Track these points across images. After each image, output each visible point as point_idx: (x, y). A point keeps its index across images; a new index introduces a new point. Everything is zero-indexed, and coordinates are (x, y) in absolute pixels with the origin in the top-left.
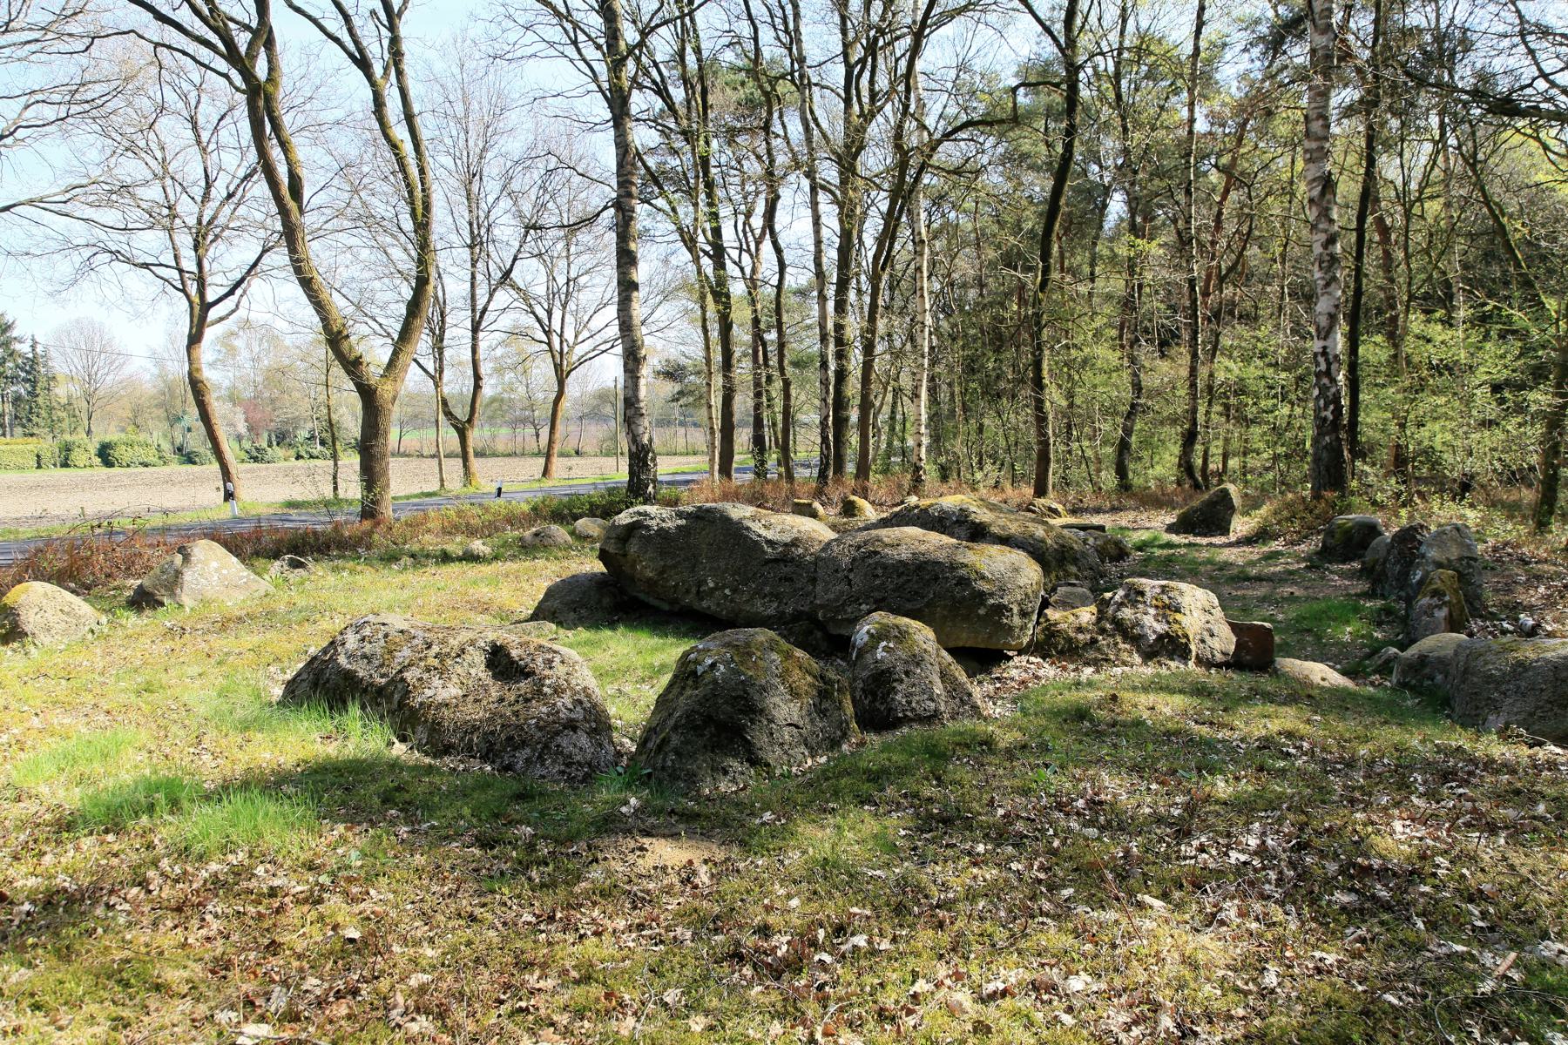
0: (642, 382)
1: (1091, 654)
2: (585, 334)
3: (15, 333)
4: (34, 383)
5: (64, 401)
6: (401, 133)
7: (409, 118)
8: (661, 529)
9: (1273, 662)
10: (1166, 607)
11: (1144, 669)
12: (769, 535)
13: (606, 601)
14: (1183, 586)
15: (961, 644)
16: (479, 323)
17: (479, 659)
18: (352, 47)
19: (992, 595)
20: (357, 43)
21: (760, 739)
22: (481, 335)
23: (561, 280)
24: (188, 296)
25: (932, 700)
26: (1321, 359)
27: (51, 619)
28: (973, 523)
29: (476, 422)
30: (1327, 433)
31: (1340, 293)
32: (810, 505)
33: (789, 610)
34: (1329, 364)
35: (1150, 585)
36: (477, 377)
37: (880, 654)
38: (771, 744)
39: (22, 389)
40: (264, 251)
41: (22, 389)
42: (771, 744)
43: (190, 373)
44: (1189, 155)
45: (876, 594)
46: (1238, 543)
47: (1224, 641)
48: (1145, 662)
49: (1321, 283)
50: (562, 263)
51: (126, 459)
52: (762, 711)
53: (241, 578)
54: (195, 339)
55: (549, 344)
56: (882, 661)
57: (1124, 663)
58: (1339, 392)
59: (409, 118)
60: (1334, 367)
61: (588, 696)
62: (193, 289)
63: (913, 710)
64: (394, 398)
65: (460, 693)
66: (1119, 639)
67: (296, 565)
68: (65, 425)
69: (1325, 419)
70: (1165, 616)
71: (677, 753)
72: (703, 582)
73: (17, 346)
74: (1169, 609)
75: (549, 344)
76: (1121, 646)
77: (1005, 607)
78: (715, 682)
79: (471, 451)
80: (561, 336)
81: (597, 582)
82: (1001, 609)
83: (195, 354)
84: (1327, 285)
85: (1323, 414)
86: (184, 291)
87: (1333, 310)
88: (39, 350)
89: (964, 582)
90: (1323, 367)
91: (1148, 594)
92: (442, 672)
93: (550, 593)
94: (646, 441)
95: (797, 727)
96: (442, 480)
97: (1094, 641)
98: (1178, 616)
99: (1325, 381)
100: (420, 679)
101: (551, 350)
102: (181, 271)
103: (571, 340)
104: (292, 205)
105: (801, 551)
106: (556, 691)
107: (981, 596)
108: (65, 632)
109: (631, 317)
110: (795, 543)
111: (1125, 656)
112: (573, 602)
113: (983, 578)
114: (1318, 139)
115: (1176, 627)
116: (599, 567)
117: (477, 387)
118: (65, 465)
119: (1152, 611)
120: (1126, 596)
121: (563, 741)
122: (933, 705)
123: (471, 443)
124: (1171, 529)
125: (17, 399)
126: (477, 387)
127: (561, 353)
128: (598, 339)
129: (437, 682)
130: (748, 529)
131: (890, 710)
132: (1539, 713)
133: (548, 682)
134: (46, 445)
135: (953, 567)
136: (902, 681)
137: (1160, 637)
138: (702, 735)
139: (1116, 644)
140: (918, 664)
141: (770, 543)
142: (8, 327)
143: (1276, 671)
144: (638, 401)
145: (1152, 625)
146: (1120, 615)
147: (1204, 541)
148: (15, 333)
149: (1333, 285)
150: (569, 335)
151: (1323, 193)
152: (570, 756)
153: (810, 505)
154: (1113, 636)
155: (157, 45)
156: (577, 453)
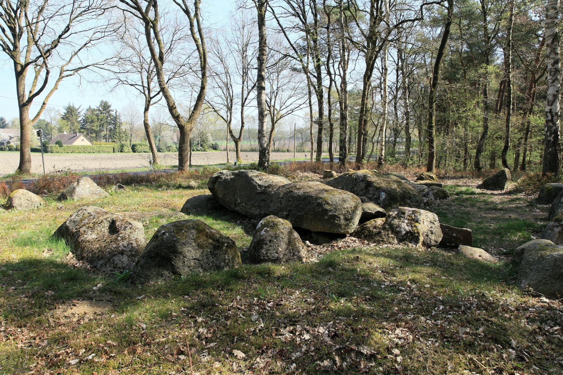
0: (265, 124)
1: (378, 238)
2: (284, 107)
3: (111, 108)
4: (115, 124)
5: (124, 130)
6: (197, 36)
7: (200, 30)
8: (225, 179)
9: (458, 246)
10: (413, 220)
11: (398, 246)
12: (260, 183)
13: (209, 205)
14: (422, 211)
15: (319, 230)
16: (244, 104)
17: (107, 225)
18: (184, 7)
19: (331, 211)
20: (185, 5)
21: (179, 264)
22: (245, 108)
23: (275, 88)
24: (145, 95)
25: (277, 253)
26: (549, 115)
27: (23, 202)
28: (368, 181)
29: (242, 139)
30: (551, 147)
31: (559, 85)
32: (331, 172)
33: (263, 213)
34: (552, 116)
35: (408, 210)
36: (243, 123)
37: (263, 232)
38: (184, 266)
39: (112, 126)
40: (169, 79)
41: (112, 126)
42: (184, 266)
43: (144, 121)
44: (509, 29)
45: (289, 208)
46: (506, 193)
47: (438, 236)
48: (399, 243)
49: (550, 81)
50: (276, 82)
51: (140, 150)
52: (181, 253)
53: (97, 191)
54: (147, 109)
55: (270, 111)
56: (262, 236)
57: (390, 243)
58: (557, 129)
59: (200, 30)
60: (555, 118)
61: (136, 241)
62: (147, 92)
63: (268, 256)
64: (191, 130)
65: (96, 237)
66: (390, 232)
67: (120, 187)
68: (124, 138)
69: (550, 141)
70: (411, 224)
71: (142, 267)
72: (236, 200)
73: (111, 113)
74: (414, 221)
75: (270, 111)
76: (390, 235)
77: (337, 216)
78: (162, 240)
79: (239, 149)
80: (274, 107)
81: (207, 199)
82: (334, 217)
83: (146, 115)
84: (553, 82)
85: (549, 139)
86: (144, 93)
87: (555, 93)
88: (118, 114)
89: (320, 205)
90: (550, 118)
91: (407, 214)
92: (92, 229)
93: (188, 202)
94: (265, 146)
95: (198, 260)
96: (228, 159)
97: (380, 233)
98: (417, 224)
99: (550, 124)
100: (85, 231)
101: (270, 113)
102: (144, 87)
103: (278, 109)
104: (159, 62)
105: (270, 189)
106: (122, 239)
107: (326, 211)
108: (27, 207)
109: (261, 100)
110: (269, 186)
111: (391, 240)
112: (195, 205)
113: (328, 203)
114: (552, 18)
115: (415, 228)
116: (208, 192)
117: (242, 126)
118: (121, 151)
119: (406, 221)
120: (398, 214)
121: (116, 258)
122: (277, 255)
123: (239, 146)
124: (479, 187)
125: (111, 130)
126: (242, 126)
127: (274, 113)
128: (289, 108)
129: (90, 232)
130: (253, 180)
131: (259, 256)
132: (544, 281)
133: (121, 235)
134: (117, 145)
135: (317, 198)
136: (267, 244)
137: (407, 233)
138: (155, 261)
139: (388, 234)
140: (276, 238)
141: (260, 186)
142: (109, 107)
143: (458, 250)
144: (263, 131)
145: (405, 226)
146: (393, 222)
147: (489, 192)
148: (111, 108)
149: (556, 82)
150: (277, 107)
151: (553, 42)
152: (116, 265)
153: (331, 172)
154: (388, 231)
155: (124, 10)
156: (288, 151)
